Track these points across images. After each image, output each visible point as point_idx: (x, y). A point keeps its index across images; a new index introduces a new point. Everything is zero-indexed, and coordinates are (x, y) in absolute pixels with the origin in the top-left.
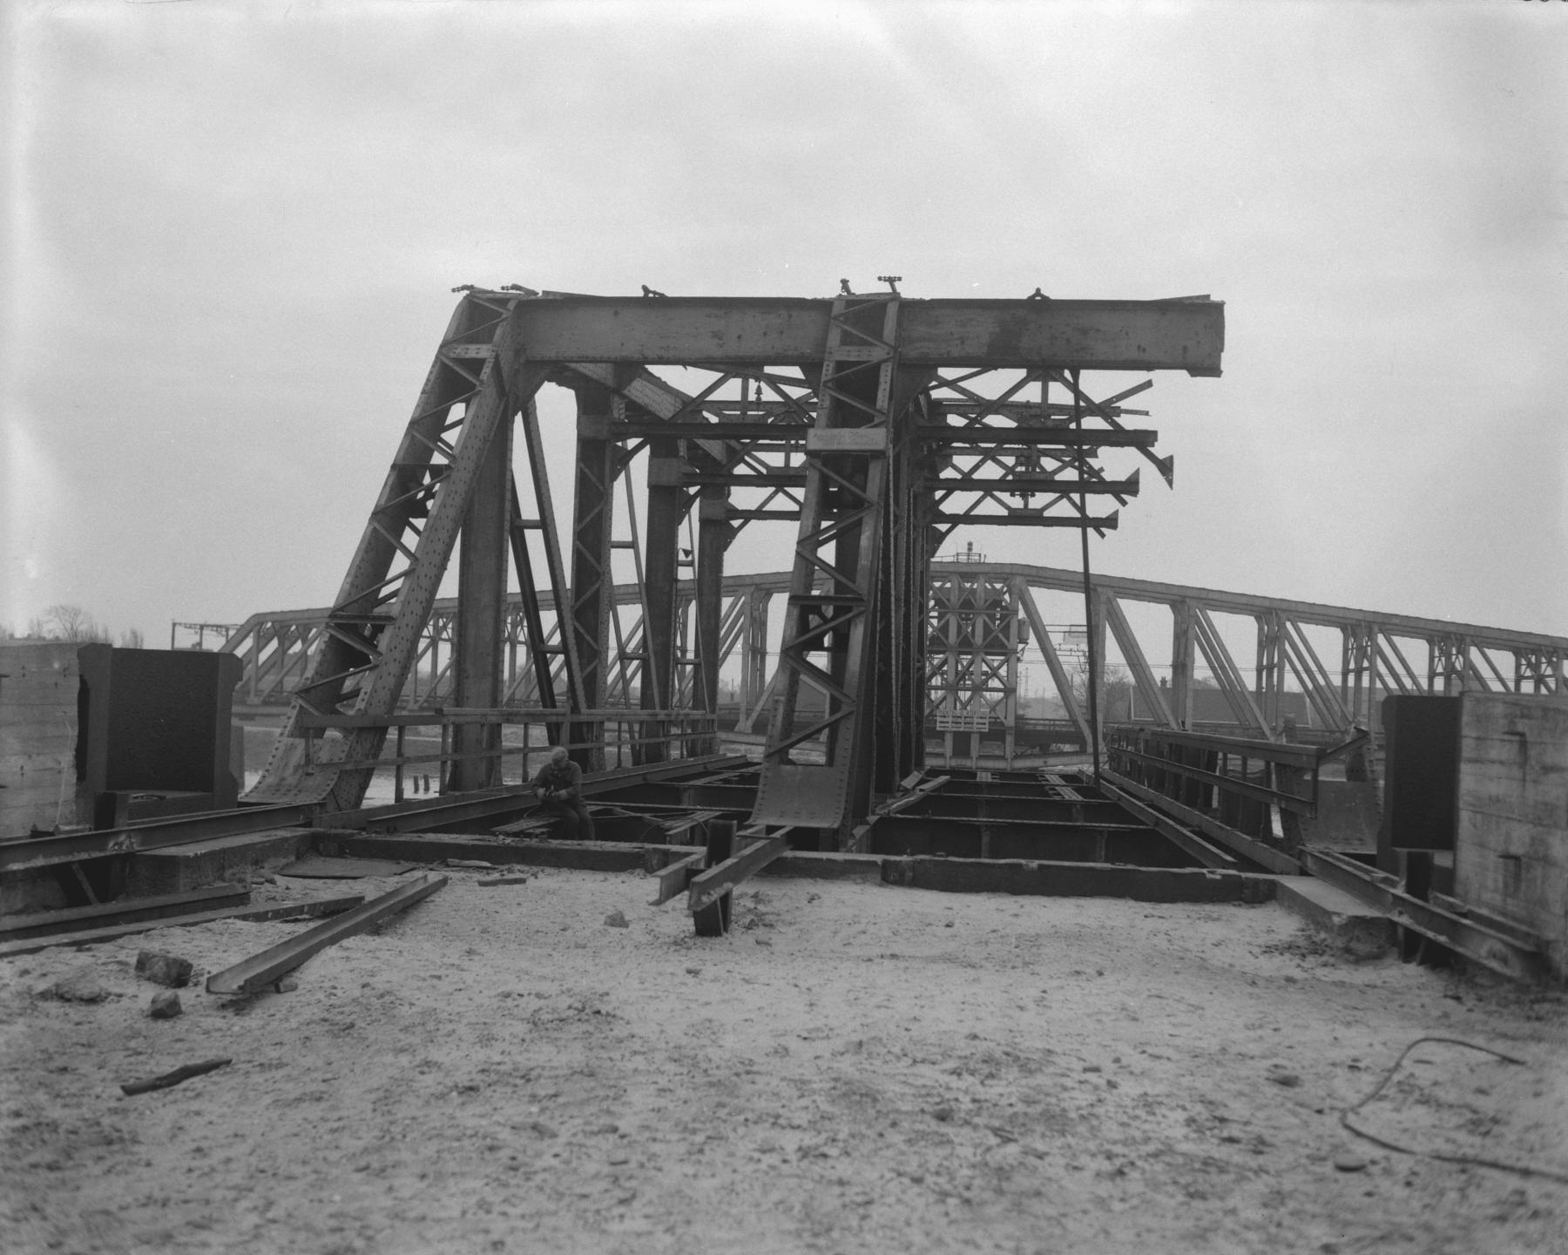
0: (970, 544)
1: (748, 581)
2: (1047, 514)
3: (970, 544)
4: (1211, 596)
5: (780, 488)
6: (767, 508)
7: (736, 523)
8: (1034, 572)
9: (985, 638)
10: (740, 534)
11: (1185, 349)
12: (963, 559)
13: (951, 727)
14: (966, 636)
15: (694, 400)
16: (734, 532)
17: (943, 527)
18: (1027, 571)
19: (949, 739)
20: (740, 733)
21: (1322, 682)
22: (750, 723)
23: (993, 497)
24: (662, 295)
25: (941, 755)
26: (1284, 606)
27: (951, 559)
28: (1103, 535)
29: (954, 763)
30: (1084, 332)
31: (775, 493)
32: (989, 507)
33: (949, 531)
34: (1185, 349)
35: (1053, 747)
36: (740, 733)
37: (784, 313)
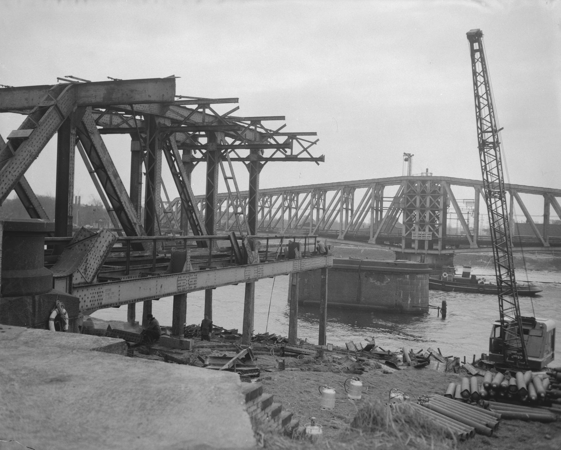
0: (427, 169)
1: (342, 184)
2: (298, 157)
3: (427, 169)
4: (520, 187)
5: (278, 149)
6: (274, 157)
7: (194, 163)
8: (449, 179)
9: (430, 205)
10: (196, 168)
11: (163, 95)
12: (425, 175)
13: (417, 238)
14: (423, 204)
15: (220, 117)
16: (194, 166)
17: (263, 163)
18: (446, 179)
19: (416, 242)
20: (340, 240)
21: (397, 216)
22: (343, 236)
23: (234, 152)
24: (8, 86)
25: (437, 250)
26: (550, 191)
27: (420, 175)
28: (318, 164)
29: (419, 251)
30: (132, 91)
31: (276, 151)
32: (279, 155)
33: (265, 164)
34: (163, 95)
35: (460, 246)
36: (340, 240)
37: (44, 90)
